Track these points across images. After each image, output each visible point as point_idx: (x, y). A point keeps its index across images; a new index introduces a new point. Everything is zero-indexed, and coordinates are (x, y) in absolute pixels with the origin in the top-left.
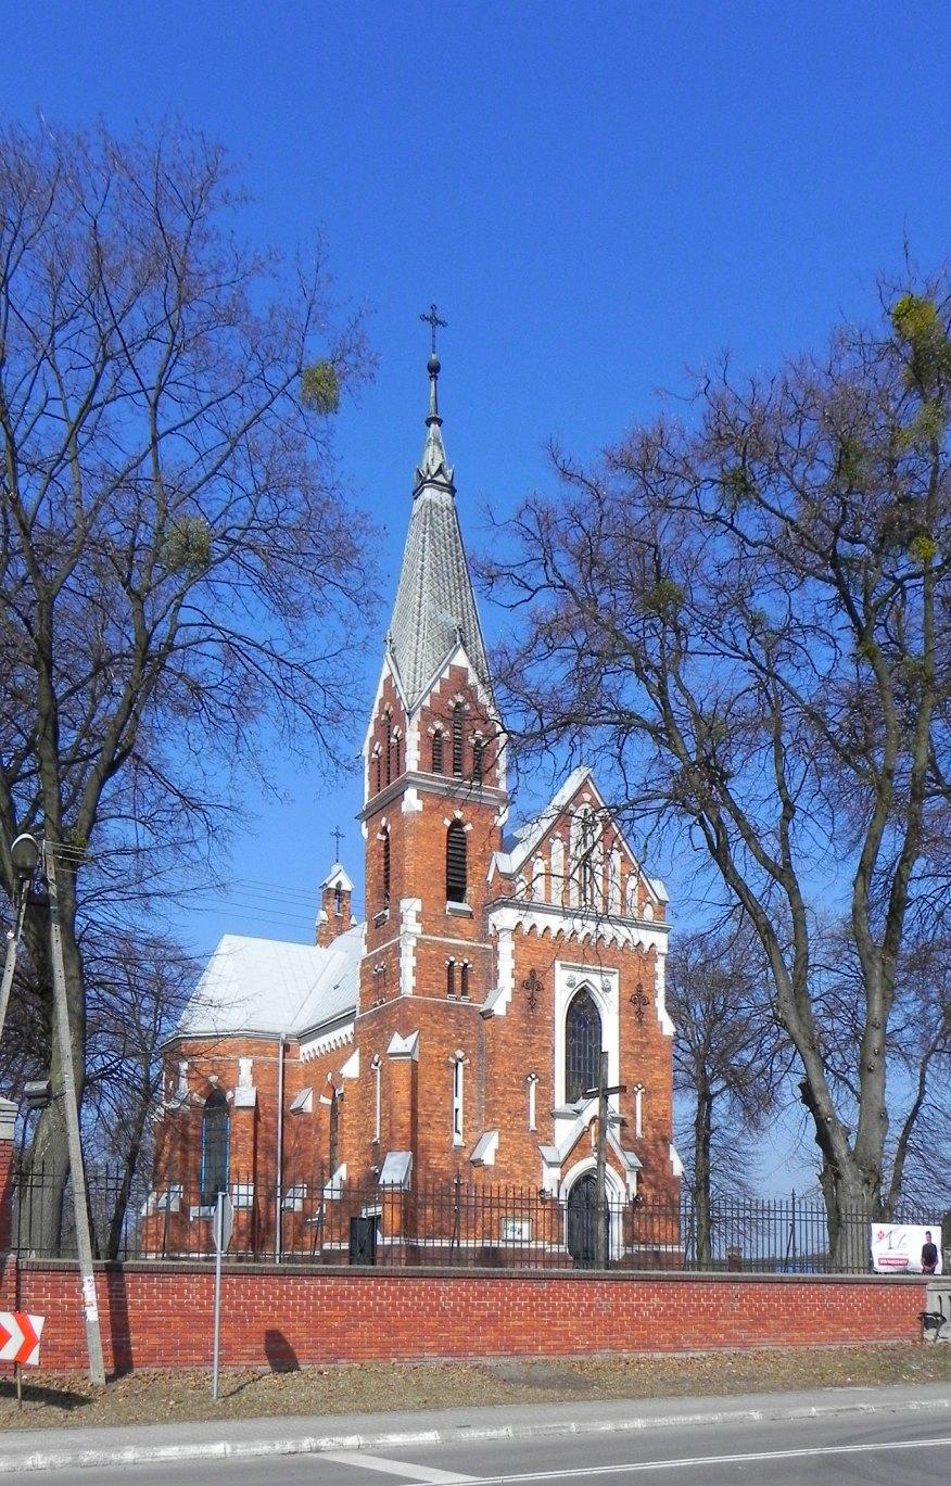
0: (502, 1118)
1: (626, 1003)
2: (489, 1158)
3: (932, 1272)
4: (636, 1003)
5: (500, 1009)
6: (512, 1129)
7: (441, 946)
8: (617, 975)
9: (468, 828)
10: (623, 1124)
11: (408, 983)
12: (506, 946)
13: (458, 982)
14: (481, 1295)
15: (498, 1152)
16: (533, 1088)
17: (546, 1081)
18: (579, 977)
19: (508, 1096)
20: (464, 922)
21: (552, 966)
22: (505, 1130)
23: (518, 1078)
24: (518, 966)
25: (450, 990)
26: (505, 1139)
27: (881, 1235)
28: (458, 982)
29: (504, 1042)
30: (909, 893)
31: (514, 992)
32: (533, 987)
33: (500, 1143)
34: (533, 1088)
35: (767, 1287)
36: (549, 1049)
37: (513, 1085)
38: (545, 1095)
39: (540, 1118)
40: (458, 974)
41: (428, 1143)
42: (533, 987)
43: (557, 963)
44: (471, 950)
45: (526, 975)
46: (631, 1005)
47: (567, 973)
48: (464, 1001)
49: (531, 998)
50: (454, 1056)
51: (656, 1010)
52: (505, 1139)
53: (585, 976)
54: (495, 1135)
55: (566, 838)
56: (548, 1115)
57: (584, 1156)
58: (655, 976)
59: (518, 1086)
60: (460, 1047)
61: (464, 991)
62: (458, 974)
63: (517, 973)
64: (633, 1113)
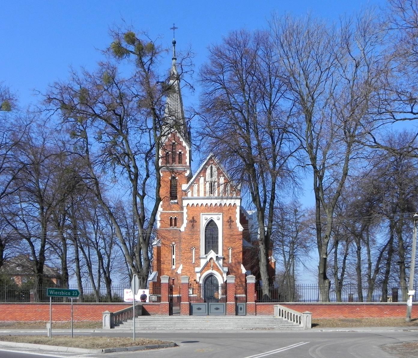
0: (183, 260)
1: (225, 223)
2: (179, 271)
3: (145, 302)
4: (230, 222)
5: (182, 229)
6: (186, 263)
7: (168, 213)
8: (221, 215)
9: (177, 178)
10: (224, 259)
11: (159, 225)
12: (185, 211)
13: (173, 223)
14: (8, 308)
15: (182, 270)
16: (194, 251)
17: (198, 249)
18: (209, 217)
19: (185, 254)
20: (176, 206)
21: (200, 215)
22: (184, 263)
23: (188, 248)
24: (188, 216)
25: (171, 225)
26: (184, 266)
27: (127, 293)
28: (173, 223)
29: (184, 239)
30: (369, 168)
31: (187, 224)
32: (193, 222)
33: (183, 267)
34: (194, 251)
35: (86, 306)
36: (198, 239)
37: (186, 250)
38: (198, 253)
39: (196, 259)
40: (173, 221)
41: (164, 268)
42: (193, 222)
43: (201, 214)
44: (177, 213)
45: (191, 219)
46: (227, 223)
47: (204, 216)
48: (175, 228)
49: (193, 225)
50: (172, 244)
51: (236, 224)
52: (184, 266)
53: (210, 216)
54: (182, 265)
55: (204, 176)
56: (198, 258)
57: (208, 269)
58: (236, 213)
59: (188, 251)
60: (174, 241)
61: (175, 225)
62: (173, 221)
63: (188, 218)
64: (228, 256)
